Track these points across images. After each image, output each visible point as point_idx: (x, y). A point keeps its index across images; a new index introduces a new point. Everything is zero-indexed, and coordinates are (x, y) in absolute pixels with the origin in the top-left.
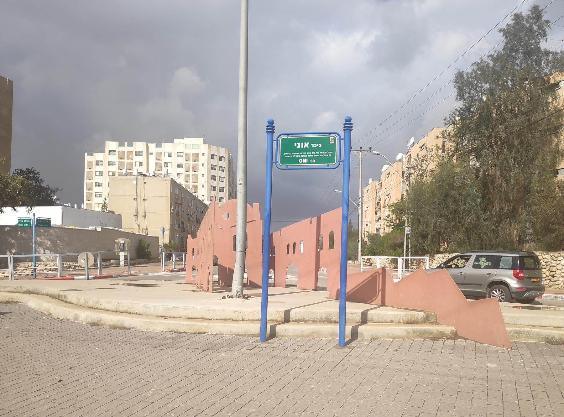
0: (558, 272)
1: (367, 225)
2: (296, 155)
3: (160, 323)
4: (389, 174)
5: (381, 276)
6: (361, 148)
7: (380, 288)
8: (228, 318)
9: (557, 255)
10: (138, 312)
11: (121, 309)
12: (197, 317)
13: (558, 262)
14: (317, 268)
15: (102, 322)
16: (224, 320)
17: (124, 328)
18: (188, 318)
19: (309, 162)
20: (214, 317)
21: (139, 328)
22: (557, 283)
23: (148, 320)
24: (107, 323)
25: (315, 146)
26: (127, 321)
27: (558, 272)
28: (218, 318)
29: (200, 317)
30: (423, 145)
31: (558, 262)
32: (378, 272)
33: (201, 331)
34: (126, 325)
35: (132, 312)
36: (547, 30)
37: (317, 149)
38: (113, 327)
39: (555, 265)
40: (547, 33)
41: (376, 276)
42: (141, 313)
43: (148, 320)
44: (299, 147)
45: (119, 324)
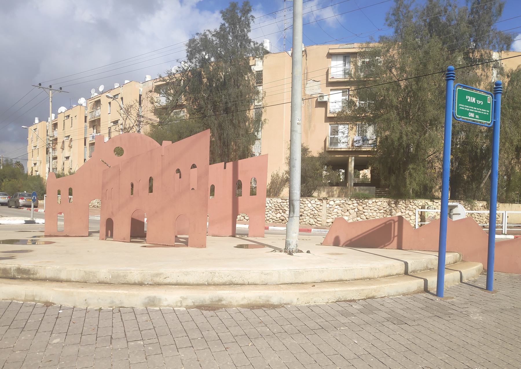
0: (305, 212)
1: (35, 164)
2: (467, 108)
3: (324, 292)
4: (68, 116)
5: (397, 224)
6: (61, 88)
7: (396, 234)
8: (366, 276)
9: (305, 200)
10: (251, 281)
11: (216, 280)
12: (335, 279)
13: (306, 205)
14: (235, 212)
15: (224, 302)
16: (361, 279)
17: (274, 307)
18: (324, 282)
19: (475, 118)
20: (352, 277)
21: (295, 302)
22: (304, 220)
23: (306, 291)
24: (235, 303)
25: (479, 102)
26: (276, 296)
27: (305, 212)
28: (356, 277)
29: (338, 278)
30: (118, 95)
31: (306, 205)
32: (393, 220)
33: (371, 296)
34: (275, 300)
35: (240, 282)
36: (252, 22)
37: (479, 106)
38: (252, 307)
39: (303, 207)
40: (251, 25)
41: (391, 224)
42: (258, 282)
43: (306, 291)
44: (469, 101)
45: (261, 302)
